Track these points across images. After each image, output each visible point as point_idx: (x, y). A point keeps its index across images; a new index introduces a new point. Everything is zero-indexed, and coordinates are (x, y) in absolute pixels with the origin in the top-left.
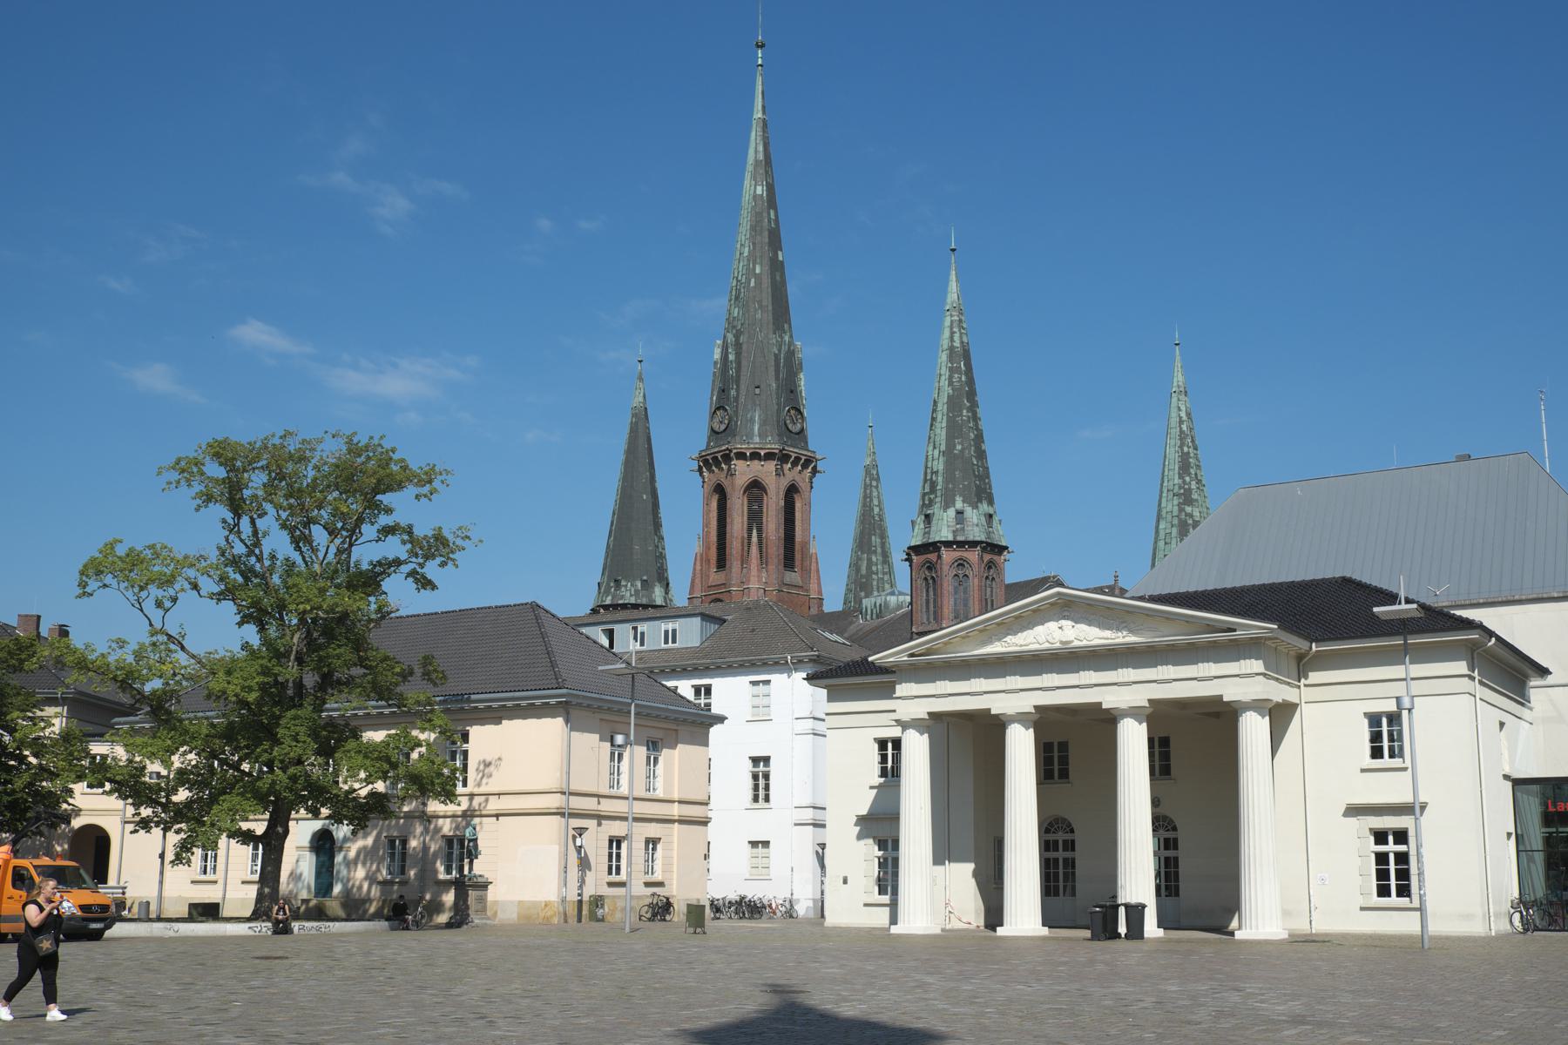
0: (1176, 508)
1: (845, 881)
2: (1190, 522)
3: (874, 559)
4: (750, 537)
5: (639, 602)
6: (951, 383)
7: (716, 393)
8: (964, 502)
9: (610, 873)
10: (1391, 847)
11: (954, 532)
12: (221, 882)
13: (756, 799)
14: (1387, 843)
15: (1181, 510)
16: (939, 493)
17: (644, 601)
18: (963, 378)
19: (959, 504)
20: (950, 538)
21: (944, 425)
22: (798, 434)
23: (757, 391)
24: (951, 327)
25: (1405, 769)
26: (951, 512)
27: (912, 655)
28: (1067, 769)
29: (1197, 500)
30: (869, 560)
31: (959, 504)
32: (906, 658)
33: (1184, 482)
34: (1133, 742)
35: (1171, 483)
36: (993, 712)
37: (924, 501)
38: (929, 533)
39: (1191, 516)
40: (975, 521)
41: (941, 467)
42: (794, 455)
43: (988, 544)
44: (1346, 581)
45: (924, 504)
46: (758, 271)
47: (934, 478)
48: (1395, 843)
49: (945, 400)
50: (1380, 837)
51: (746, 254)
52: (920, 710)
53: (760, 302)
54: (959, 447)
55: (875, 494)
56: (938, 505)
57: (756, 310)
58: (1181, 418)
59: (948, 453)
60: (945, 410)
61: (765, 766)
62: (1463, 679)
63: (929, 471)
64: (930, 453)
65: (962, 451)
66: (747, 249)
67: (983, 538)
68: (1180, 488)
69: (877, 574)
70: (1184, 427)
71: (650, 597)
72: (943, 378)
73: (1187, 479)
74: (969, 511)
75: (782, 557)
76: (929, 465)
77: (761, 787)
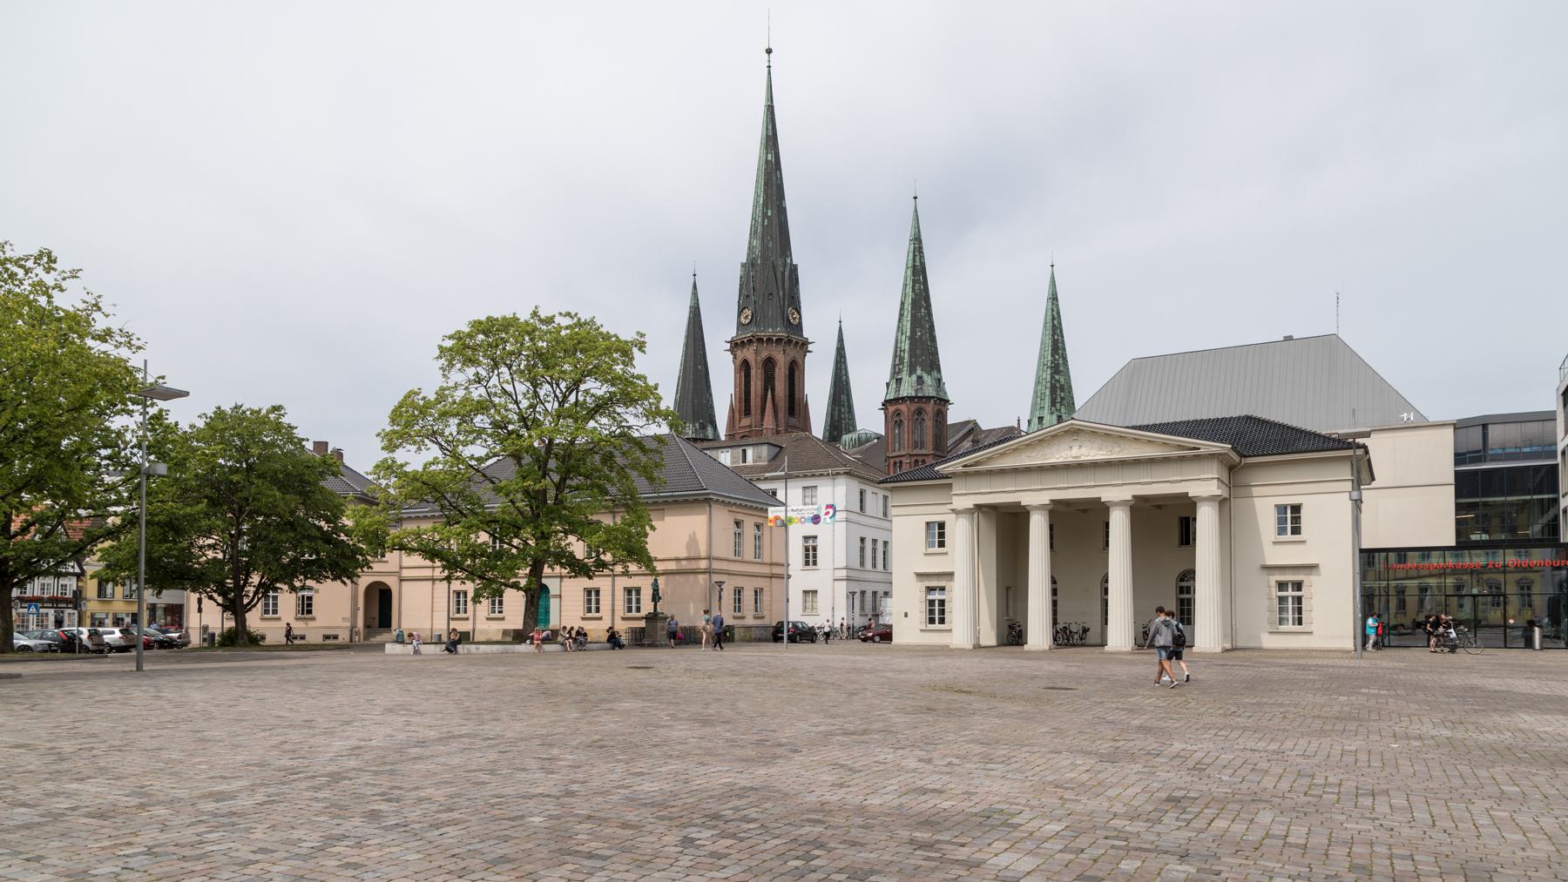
0: (1049, 377)
1: (906, 615)
2: (1058, 385)
3: (843, 410)
4: (766, 395)
5: (698, 437)
6: (913, 290)
7: (742, 298)
8: (922, 370)
9: (735, 611)
10: (1290, 593)
11: (916, 390)
12: (471, 618)
13: (807, 563)
14: (1287, 591)
15: (1052, 377)
16: (905, 365)
17: (701, 436)
18: (922, 287)
19: (919, 372)
20: (914, 394)
21: (909, 319)
22: (796, 326)
23: (771, 297)
24: (914, 252)
25: (467, 619)
26: (914, 377)
27: (964, 466)
28: (1278, 524)
29: (1062, 371)
30: (840, 411)
31: (919, 372)
32: (961, 468)
33: (1055, 359)
34: (1119, 524)
35: (1046, 360)
36: (1022, 504)
37: (895, 369)
38: (899, 391)
39: (1058, 381)
40: (930, 383)
41: (907, 347)
42: (794, 340)
43: (938, 399)
44: (1249, 418)
45: (895, 373)
46: (769, 214)
47: (902, 354)
48: (1293, 591)
49: (910, 302)
50: (1282, 586)
51: (761, 202)
52: (968, 502)
53: (771, 236)
54: (919, 334)
55: (843, 367)
56: (905, 372)
57: (768, 241)
58: (1053, 316)
59: (912, 338)
60: (910, 309)
61: (814, 542)
62: (427, 582)
63: (898, 350)
64: (899, 337)
65: (921, 336)
66: (762, 199)
67: (934, 394)
68: (1052, 363)
69: (845, 420)
70: (1056, 322)
71: (704, 434)
72: (908, 287)
73: (1057, 357)
74: (926, 377)
75: (787, 408)
76: (899, 345)
77: (810, 557)
